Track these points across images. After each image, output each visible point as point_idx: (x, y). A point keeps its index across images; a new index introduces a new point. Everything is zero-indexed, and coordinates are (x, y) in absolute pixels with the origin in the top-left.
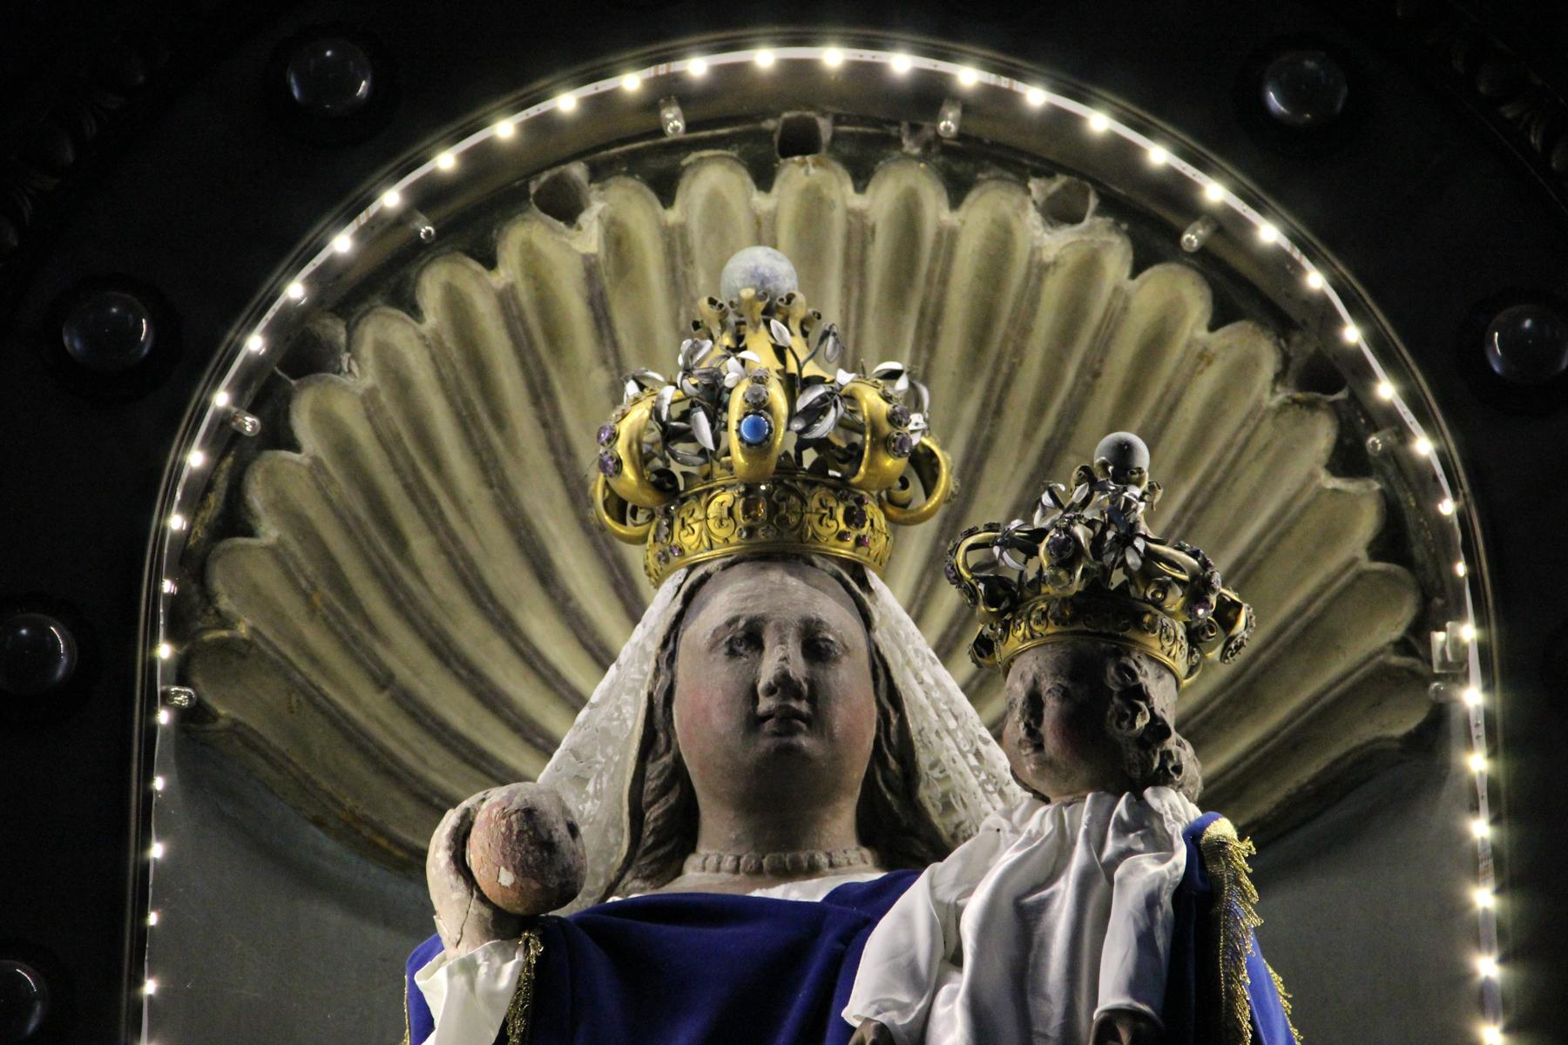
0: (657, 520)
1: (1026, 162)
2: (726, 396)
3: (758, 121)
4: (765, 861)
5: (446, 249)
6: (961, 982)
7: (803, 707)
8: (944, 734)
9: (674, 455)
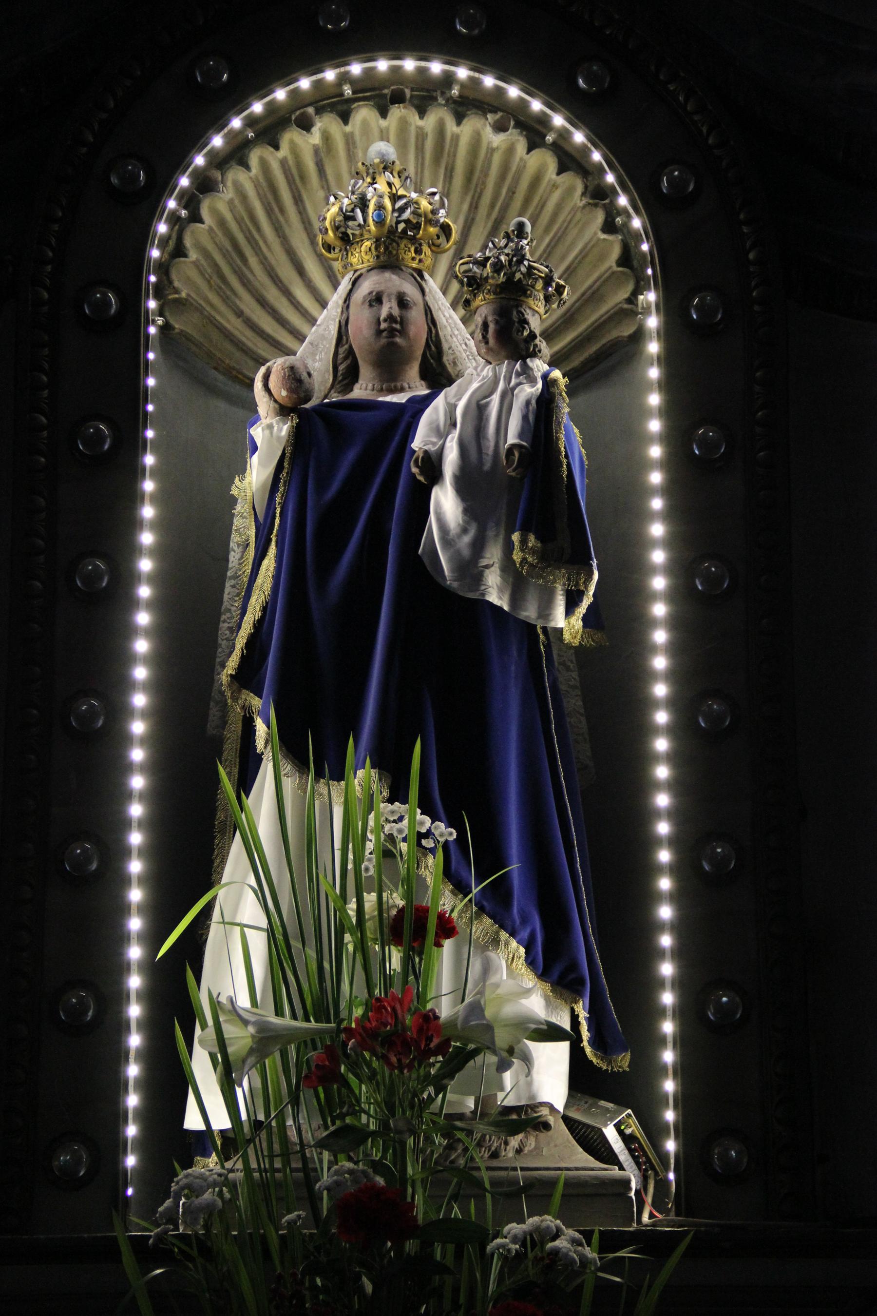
0: (342, 252)
1: (486, 107)
2: (368, 203)
3: (381, 90)
4: (384, 386)
5: (260, 142)
6: (455, 434)
7: (398, 326)
8: (453, 336)
9: (348, 226)
